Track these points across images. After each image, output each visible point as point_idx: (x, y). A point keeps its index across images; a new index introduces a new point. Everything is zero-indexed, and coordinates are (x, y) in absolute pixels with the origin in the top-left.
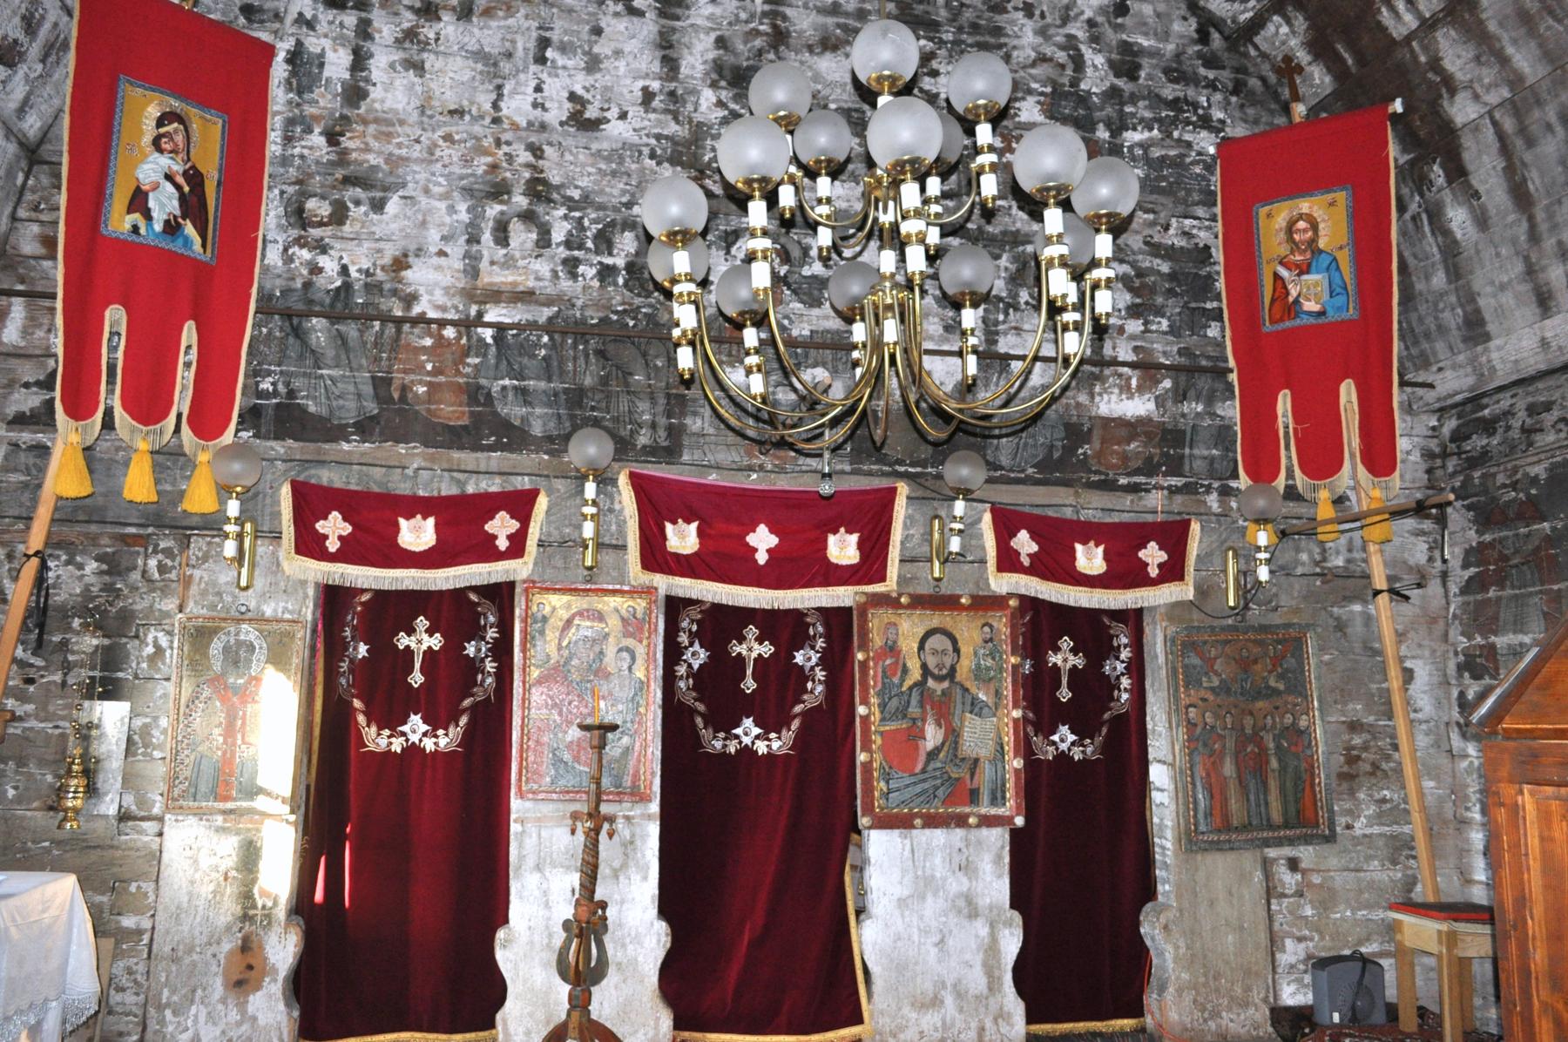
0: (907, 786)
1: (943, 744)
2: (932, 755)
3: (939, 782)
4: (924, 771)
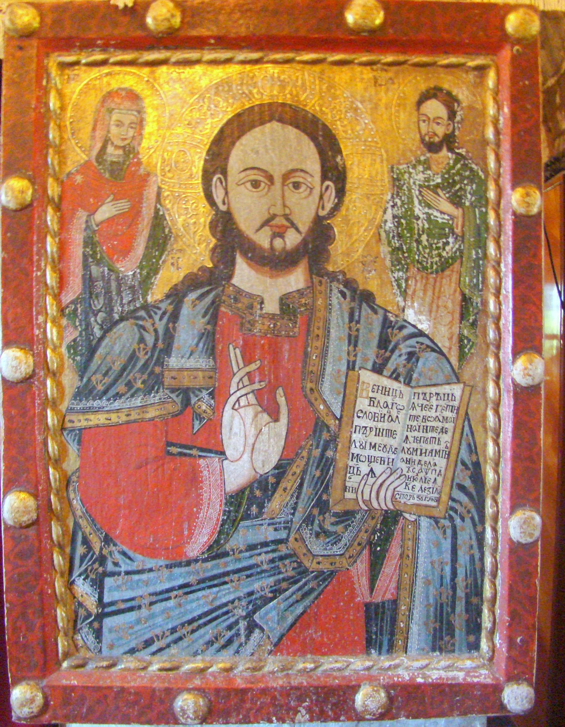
0: (163, 595)
1: (281, 469)
2: (245, 503)
4: (215, 551)
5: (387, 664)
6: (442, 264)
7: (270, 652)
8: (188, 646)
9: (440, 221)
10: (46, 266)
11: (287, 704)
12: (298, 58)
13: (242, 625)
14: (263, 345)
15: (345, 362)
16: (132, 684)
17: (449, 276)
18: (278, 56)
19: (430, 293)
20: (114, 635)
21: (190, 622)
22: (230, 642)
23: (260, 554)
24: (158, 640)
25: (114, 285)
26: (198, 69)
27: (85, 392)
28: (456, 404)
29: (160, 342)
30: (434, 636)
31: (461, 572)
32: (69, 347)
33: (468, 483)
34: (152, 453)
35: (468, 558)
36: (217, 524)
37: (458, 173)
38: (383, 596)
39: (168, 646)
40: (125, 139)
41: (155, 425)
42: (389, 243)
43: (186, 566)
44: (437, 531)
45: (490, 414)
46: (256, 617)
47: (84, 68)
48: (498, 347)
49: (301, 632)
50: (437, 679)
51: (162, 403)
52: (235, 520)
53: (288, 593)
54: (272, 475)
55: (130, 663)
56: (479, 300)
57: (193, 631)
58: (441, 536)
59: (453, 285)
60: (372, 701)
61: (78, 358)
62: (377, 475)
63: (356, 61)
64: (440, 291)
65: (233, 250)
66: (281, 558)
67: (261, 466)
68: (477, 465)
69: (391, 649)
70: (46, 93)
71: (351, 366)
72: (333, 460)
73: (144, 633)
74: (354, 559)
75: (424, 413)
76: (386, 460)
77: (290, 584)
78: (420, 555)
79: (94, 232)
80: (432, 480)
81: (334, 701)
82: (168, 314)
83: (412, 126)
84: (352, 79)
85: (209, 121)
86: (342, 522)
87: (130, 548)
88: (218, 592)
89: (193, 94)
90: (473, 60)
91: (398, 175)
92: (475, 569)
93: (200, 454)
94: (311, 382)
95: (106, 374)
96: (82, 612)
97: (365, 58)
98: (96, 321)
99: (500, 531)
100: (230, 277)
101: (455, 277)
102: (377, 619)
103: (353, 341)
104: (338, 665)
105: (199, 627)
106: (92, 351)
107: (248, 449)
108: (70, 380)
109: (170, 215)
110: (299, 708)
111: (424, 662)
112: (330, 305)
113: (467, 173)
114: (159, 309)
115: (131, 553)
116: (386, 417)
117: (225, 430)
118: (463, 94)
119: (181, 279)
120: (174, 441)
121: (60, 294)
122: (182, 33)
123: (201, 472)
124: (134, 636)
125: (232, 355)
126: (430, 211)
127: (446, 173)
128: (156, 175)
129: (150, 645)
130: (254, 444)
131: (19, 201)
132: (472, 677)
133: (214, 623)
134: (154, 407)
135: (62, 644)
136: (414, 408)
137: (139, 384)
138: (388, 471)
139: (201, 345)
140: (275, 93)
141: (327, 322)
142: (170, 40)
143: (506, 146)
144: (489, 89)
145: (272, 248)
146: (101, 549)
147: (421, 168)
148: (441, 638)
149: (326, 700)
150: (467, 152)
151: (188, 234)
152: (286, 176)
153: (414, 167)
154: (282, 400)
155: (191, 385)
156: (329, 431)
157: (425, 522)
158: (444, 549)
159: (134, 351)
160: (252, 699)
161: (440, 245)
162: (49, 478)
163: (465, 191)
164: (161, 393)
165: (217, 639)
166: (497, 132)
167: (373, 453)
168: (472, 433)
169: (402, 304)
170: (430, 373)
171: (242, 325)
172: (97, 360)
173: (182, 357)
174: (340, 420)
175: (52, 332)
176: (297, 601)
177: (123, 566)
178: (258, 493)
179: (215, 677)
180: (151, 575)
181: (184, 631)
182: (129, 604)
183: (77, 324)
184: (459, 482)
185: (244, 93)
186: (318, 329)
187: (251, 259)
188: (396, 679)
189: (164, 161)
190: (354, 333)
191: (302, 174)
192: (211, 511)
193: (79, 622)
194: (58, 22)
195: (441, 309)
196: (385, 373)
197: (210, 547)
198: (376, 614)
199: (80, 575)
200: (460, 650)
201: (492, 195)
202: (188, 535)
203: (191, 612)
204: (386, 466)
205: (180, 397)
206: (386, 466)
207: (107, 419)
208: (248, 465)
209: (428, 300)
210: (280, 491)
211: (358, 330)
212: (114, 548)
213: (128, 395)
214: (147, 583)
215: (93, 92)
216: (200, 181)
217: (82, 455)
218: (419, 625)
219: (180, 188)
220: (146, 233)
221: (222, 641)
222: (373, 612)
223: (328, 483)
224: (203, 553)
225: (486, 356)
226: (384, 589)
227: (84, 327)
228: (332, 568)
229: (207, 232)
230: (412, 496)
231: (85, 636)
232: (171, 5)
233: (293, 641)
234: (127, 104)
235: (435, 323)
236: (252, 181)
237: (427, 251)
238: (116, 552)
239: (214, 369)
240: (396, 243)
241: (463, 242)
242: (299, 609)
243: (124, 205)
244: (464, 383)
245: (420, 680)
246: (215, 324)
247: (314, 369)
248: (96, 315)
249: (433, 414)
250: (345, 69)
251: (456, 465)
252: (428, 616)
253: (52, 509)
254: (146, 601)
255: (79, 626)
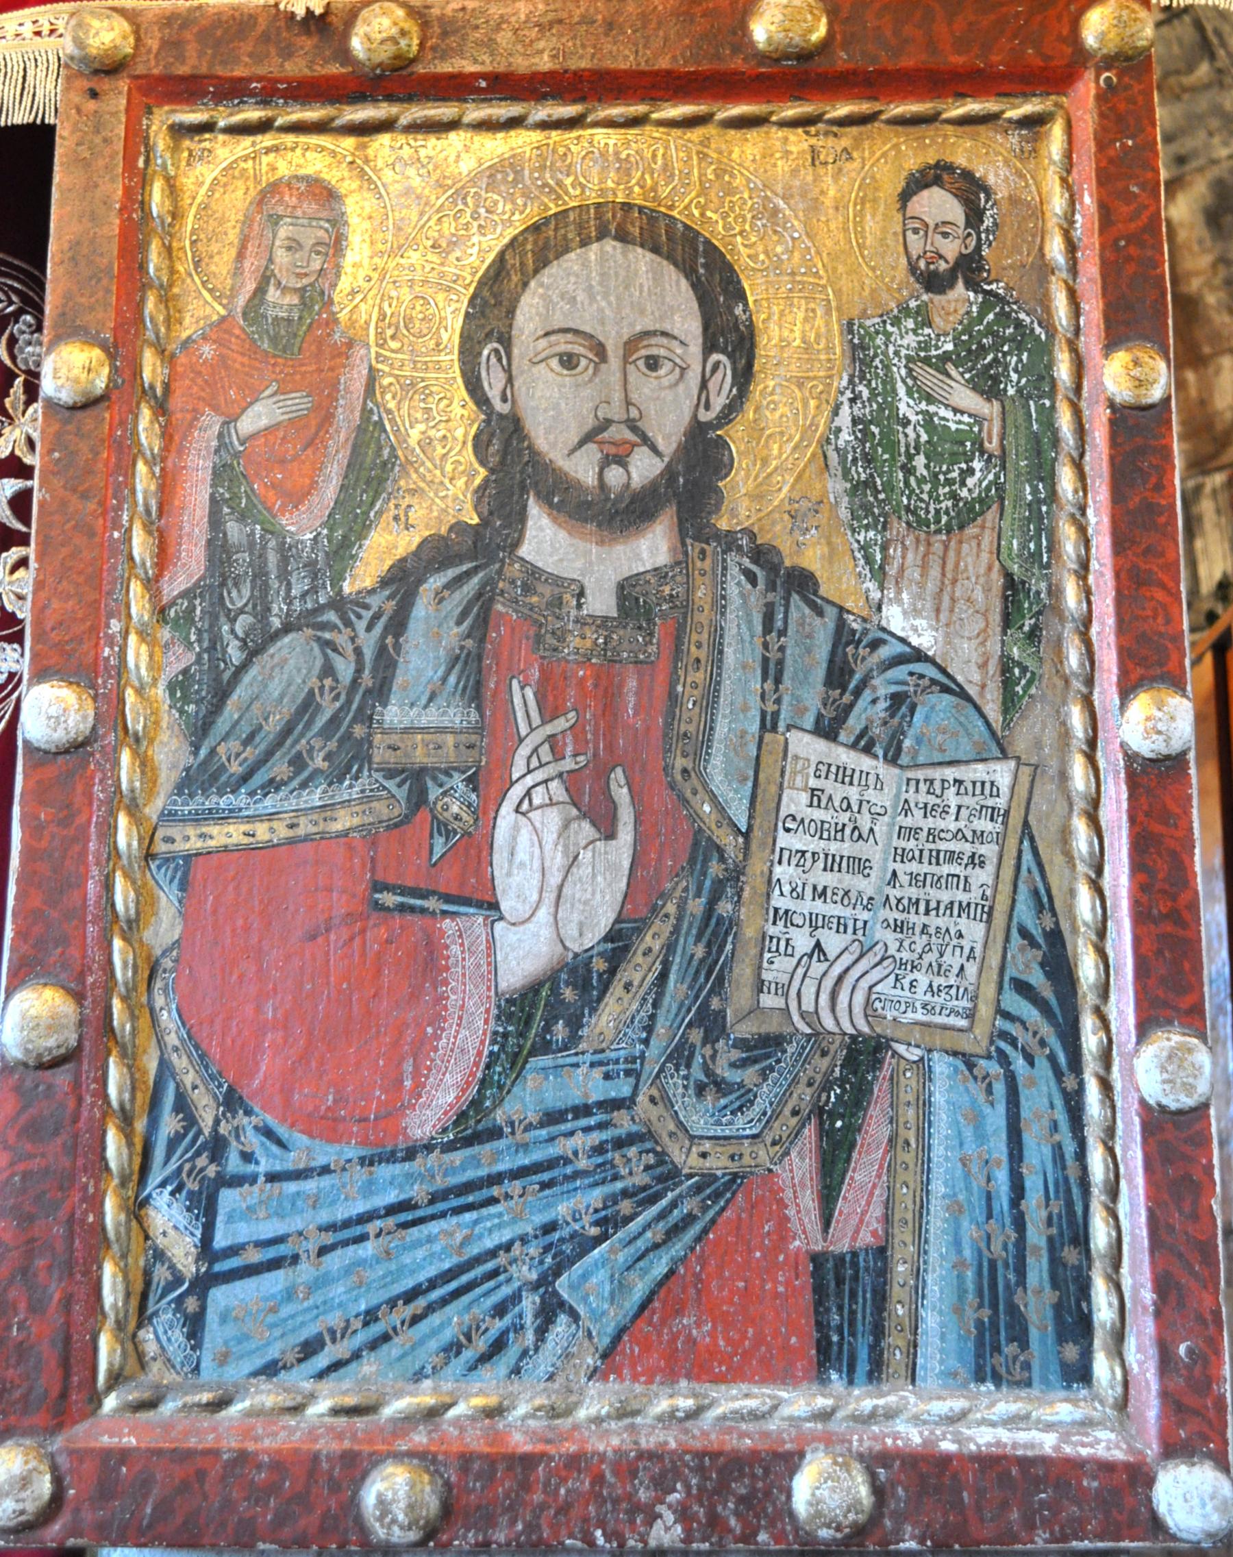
0: (348, 1232)
1: (619, 942)
2: (538, 1017)
4: (471, 1126)
5: (867, 1405)
9: (953, 427)
10: (131, 521)
12: (654, 116)
13: (529, 1304)
14: (583, 679)
15: (755, 714)
16: (267, 1443)
19: (935, 572)
20: (230, 1330)
21: (410, 1296)
22: (498, 1346)
23: (571, 1133)
24: (334, 1341)
25: (272, 559)
26: (456, 138)
27: (201, 778)
28: (1001, 803)
29: (367, 673)
30: (980, 1343)
32: (171, 687)
33: (1037, 978)
34: (340, 905)
35: (1047, 1151)
36: (476, 1064)
37: (989, 331)
38: (854, 1239)
39: (356, 1356)
41: (350, 848)
42: (846, 474)
43: (404, 1160)
44: (971, 1084)
45: (1080, 826)
46: (562, 1285)
47: (221, 137)
48: (1090, 682)
50: (989, 1445)
51: (366, 799)
52: (516, 1055)
53: (633, 1226)
54: (600, 954)
55: (267, 1396)
56: (1043, 586)
57: (415, 1320)
58: (982, 1098)
59: (985, 556)
60: (833, 1490)
61: (191, 708)
62: (831, 957)
65: (523, 489)
66: (619, 1143)
67: (576, 933)
68: (1055, 938)
69: (877, 1371)
70: (145, 181)
71: (769, 723)
72: (734, 922)
73: (303, 1324)
74: (783, 1146)
75: (930, 822)
76: (850, 924)
78: (935, 1142)
79: (237, 455)
80: (955, 970)
81: (743, 1491)
82: (384, 620)
84: (767, 154)
85: (475, 239)
86: (755, 1061)
87: (283, 1120)
88: (476, 1222)
89: (445, 188)
90: (1014, 107)
91: (861, 338)
92: (1066, 1179)
93: (445, 907)
94: (685, 755)
96: (161, 1274)
97: (792, 111)
98: (233, 631)
99: (1118, 1086)
100: (517, 544)
101: (988, 539)
102: (839, 1294)
103: (772, 671)
104: (752, 1403)
105: (430, 1309)
106: (222, 694)
107: (549, 897)
108: (170, 753)
109: (392, 421)
110: (661, 1509)
111: (958, 1404)
114: (366, 607)
115: (282, 1131)
116: (848, 831)
117: (500, 858)
118: (996, 174)
119: (414, 547)
121: (158, 577)
122: (420, 69)
123: (447, 947)
124: (277, 1332)
125: (517, 700)
126: (932, 409)
130: (561, 888)
131: (79, 388)
132: (1075, 1444)
133: (465, 1299)
134: (352, 806)
135: (107, 1350)
136: (907, 811)
137: (319, 762)
139: (452, 679)
140: (610, 184)
141: (717, 634)
142: (396, 81)
143: (1090, 269)
144: (1052, 162)
146: (217, 1122)
147: (910, 324)
148: (994, 1351)
149: (722, 1489)
150: (1008, 288)
151: (431, 460)
152: (631, 345)
153: (896, 322)
154: (622, 795)
155: (429, 761)
156: (722, 859)
157: (941, 1065)
158: (990, 1129)
159: (311, 693)
160: (547, 1484)
161: (955, 474)
162: (110, 962)
164: (364, 780)
165: (469, 1340)
166: (1071, 247)
167: (819, 907)
168: (1040, 865)
170: (940, 738)
171: (539, 639)
172: (231, 711)
173: (412, 705)
174: (747, 835)
175: (137, 654)
176: (656, 1246)
177: (263, 1161)
178: (568, 994)
179: (462, 1429)
180: (326, 1181)
181: (395, 1318)
182: (271, 1253)
183: (193, 638)
184: (1016, 974)
185: (545, 185)
186: (699, 646)
187: (559, 508)
188: (889, 1441)
189: (382, 316)
190: (773, 655)
191: (664, 341)
192: (464, 1033)
193: (152, 1299)
194: (172, 45)
195: (961, 604)
196: (842, 737)
197: (462, 1116)
198: (839, 1282)
199: (163, 1185)
200: (1045, 1381)
201: (1063, 371)
202: (412, 1091)
203: (413, 1272)
204: (849, 936)
206: (849, 936)
207: (246, 834)
208: (546, 933)
209: (931, 586)
210: (617, 989)
211: (782, 649)
212: (246, 1120)
213: (295, 784)
215: (240, 183)
216: (455, 357)
217: (187, 914)
218: (941, 1313)
219: (415, 369)
220: (343, 456)
222: (831, 1276)
224: (445, 1130)
225: (1064, 703)
226: (854, 1221)
227: (206, 644)
228: (734, 1167)
229: (469, 454)
231: (163, 1334)
232: (400, 13)
233: (646, 1347)
234: (310, 207)
235: (947, 635)
236: (561, 355)
238: (250, 1132)
239: (479, 729)
240: (860, 472)
241: (1004, 467)
242: (660, 1267)
243: (298, 402)
244: (1018, 758)
245: (948, 1446)
246: (482, 640)
247: (692, 729)
248: (233, 621)
249: (950, 824)
250: (753, 134)
251: (1007, 939)
252: (962, 1292)
253: (112, 1030)
254: (312, 1246)
255: (151, 1309)
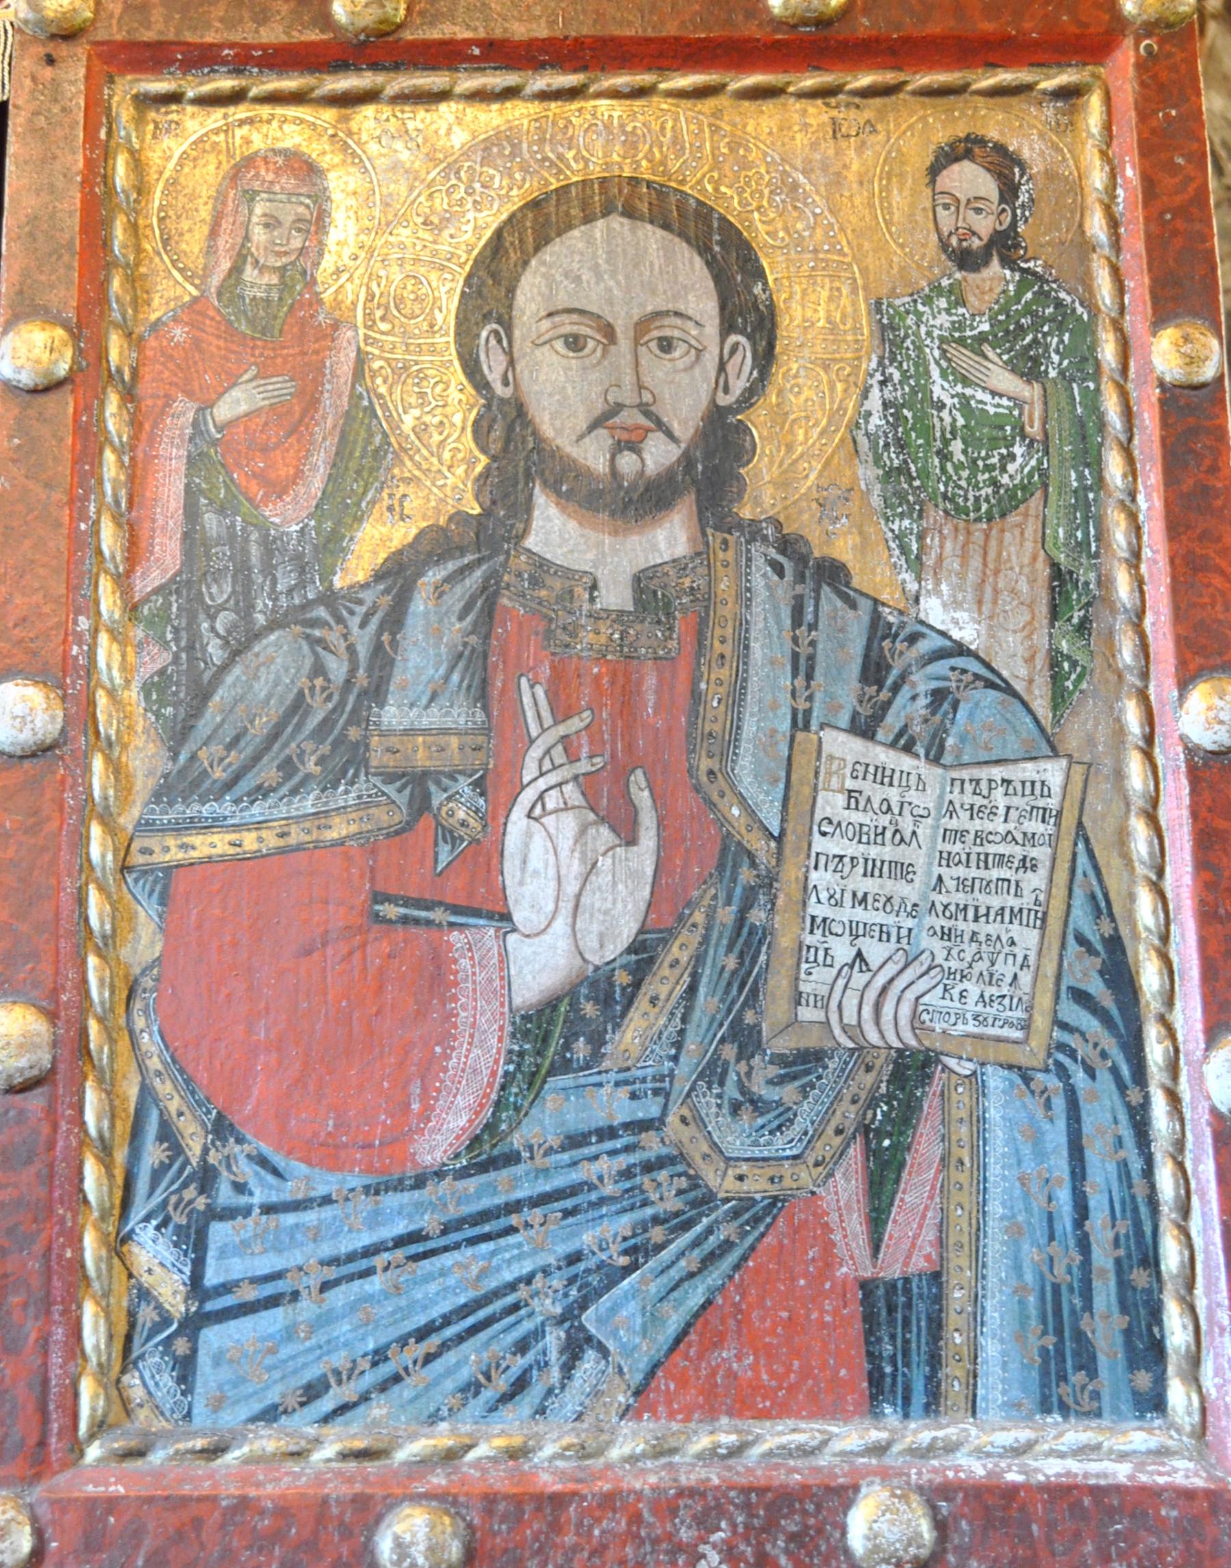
0: (355, 1265)
1: (643, 954)
2: (554, 1035)
3: (602, 1234)
4: (486, 1153)
5: (925, 1437)
6: (1000, 501)
7: (625, 1413)
8: (416, 1397)
9: (992, 410)
11: (669, 1537)
13: (554, 1339)
17: (1019, 525)
18: (622, 80)
19: (976, 562)
20: (225, 1373)
21: (422, 1334)
22: (521, 1385)
23: (596, 1157)
25: (255, 551)
26: (447, 110)
28: (1053, 803)
29: (361, 672)
30: (1045, 1373)
31: (1097, 1203)
32: (146, 689)
33: (1096, 986)
35: (1112, 1168)
36: (490, 1085)
37: (1027, 311)
39: (365, 1398)
40: (286, 253)
41: (347, 857)
42: (877, 460)
43: (413, 1188)
44: (1028, 1099)
46: (589, 1319)
47: (190, 109)
49: (700, 1356)
51: (363, 805)
52: (534, 1074)
53: (666, 1255)
54: (624, 967)
55: (267, 1441)
56: (1092, 576)
57: (429, 1359)
58: (1040, 1113)
59: (1029, 545)
61: (169, 711)
62: (874, 967)
63: (791, 89)
64: (999, 554)
66: (649, 1167)
67: (596, 945)
68: (1115, 944)
69: (934, 1403)
70: (107, 154)
71: (801, 721)
73: (305, 1365)
75: (977, 824)
76: (894, 932)
77: (672, 1230)
78: (991, 1160)
80: (1008, 979)
83: (919, 218)
85: (470, 215)
86: (795, 1077)
87: (278, 1148)
88: (493, 1253)
90: (1048, 78)
91: (891, 318)
92: (1133, 1198)
93: (453, 919)
94: (710, 756)
95: (230, 746)
96: (147, 1315)
97: (810, 81)
98: (213, 629)
101: (1032, 528)
102: (892, 1322)
104: (800, 1438)
105: (445, 1347)
106: (202, 695)
107: (566, 907)
108: (145, 758)
109: (384, 407)
110: (702, 1548)
111: (1024, 1435)
112: (748, 590)
113: (1049, 311)
114: (360, 602)
115: (278, 1160)
116: (888, 834)
119: (410, 538)
120: (392, 891)
121: (129, 573)
123: (455, 961)
124: (277, 1375)
125: (527, 700)
126: (968, 392)
127: (1000, 312)
128: (355, 327)
129: (318, 1396)
130: (578, 896)
132: (1152, 1473)
133: (483, 1336)
134: (344, 816)
136: (952, 813)
137: (311, 766)
138: (900, 958)
139: (455, 677)
140: (616, 158)
141: (743, 627)
145: (614, 472)
146: (206, 1151)
147: (943, 303)
148: (1061, 1377)
149: (771, 1526)
150: (1047, 266)
152: (642, 326)
154: (643, 798)
156: (753, 865)
157: (996, 1080)
158: (1049, 1146)
159: (301, 694)
160: (580, 1524)
161: (995, 460)
162: (85, 981)
163: (1047, 347)
164: (361, 785)
165: (489, 1378)
166: (1113, 223)
167: (860, 914)
168: (1096, 868)
169: (912, 587)
170: (985, 736)
171: (549, 634)
172: (211, 716)
173: (412, 705)
174: (779, 840)
176: (691, 1275)
178: (589, 1009)
180: (328, 1212)
182: (269, 1290)
183: (169, 636)
187: (569, 496)
190: (804, 651)
191: (678, 321)
192: (476, 1052)
193: (137, 1341)
195: (1005, 596)
196: (880, 735)
197: (476, 1140)
198: (891, 1309)
199: (147, 1219)
200: (1116, 1410)
201: (1108, 352)
205: (407, 791)
208: (564, 945)
209: (971, 577)
210: (642, 1003)
211: (813, 644)
212: (237, 1149)
213: (284, 790)
214: (316, 1235)
215: (212, 158)
218: (1002, 1341)
219: (407, 351)
221: (502, 1383)
222: (882, 1304)
223: (756, 982)
224: (457, 1156)
226: (906, 1245)
228: (773, 1190)
230: (961, 1017)
231: (151, 1379)
233: (683, 1382)
235: (990, 627)
236: (566, 337)
237: (965, 474)
238: (243, 1161)
239: (486, 730)
242: (695, 1296)
243: (281, 387)
244: (1070, 756)
246: (487, 637)
247: (717, 728)
248: (212, 618)
250: (768, 106)
251: (1063, 946)
252: (1023, 1318)
254: (314, 1281)
